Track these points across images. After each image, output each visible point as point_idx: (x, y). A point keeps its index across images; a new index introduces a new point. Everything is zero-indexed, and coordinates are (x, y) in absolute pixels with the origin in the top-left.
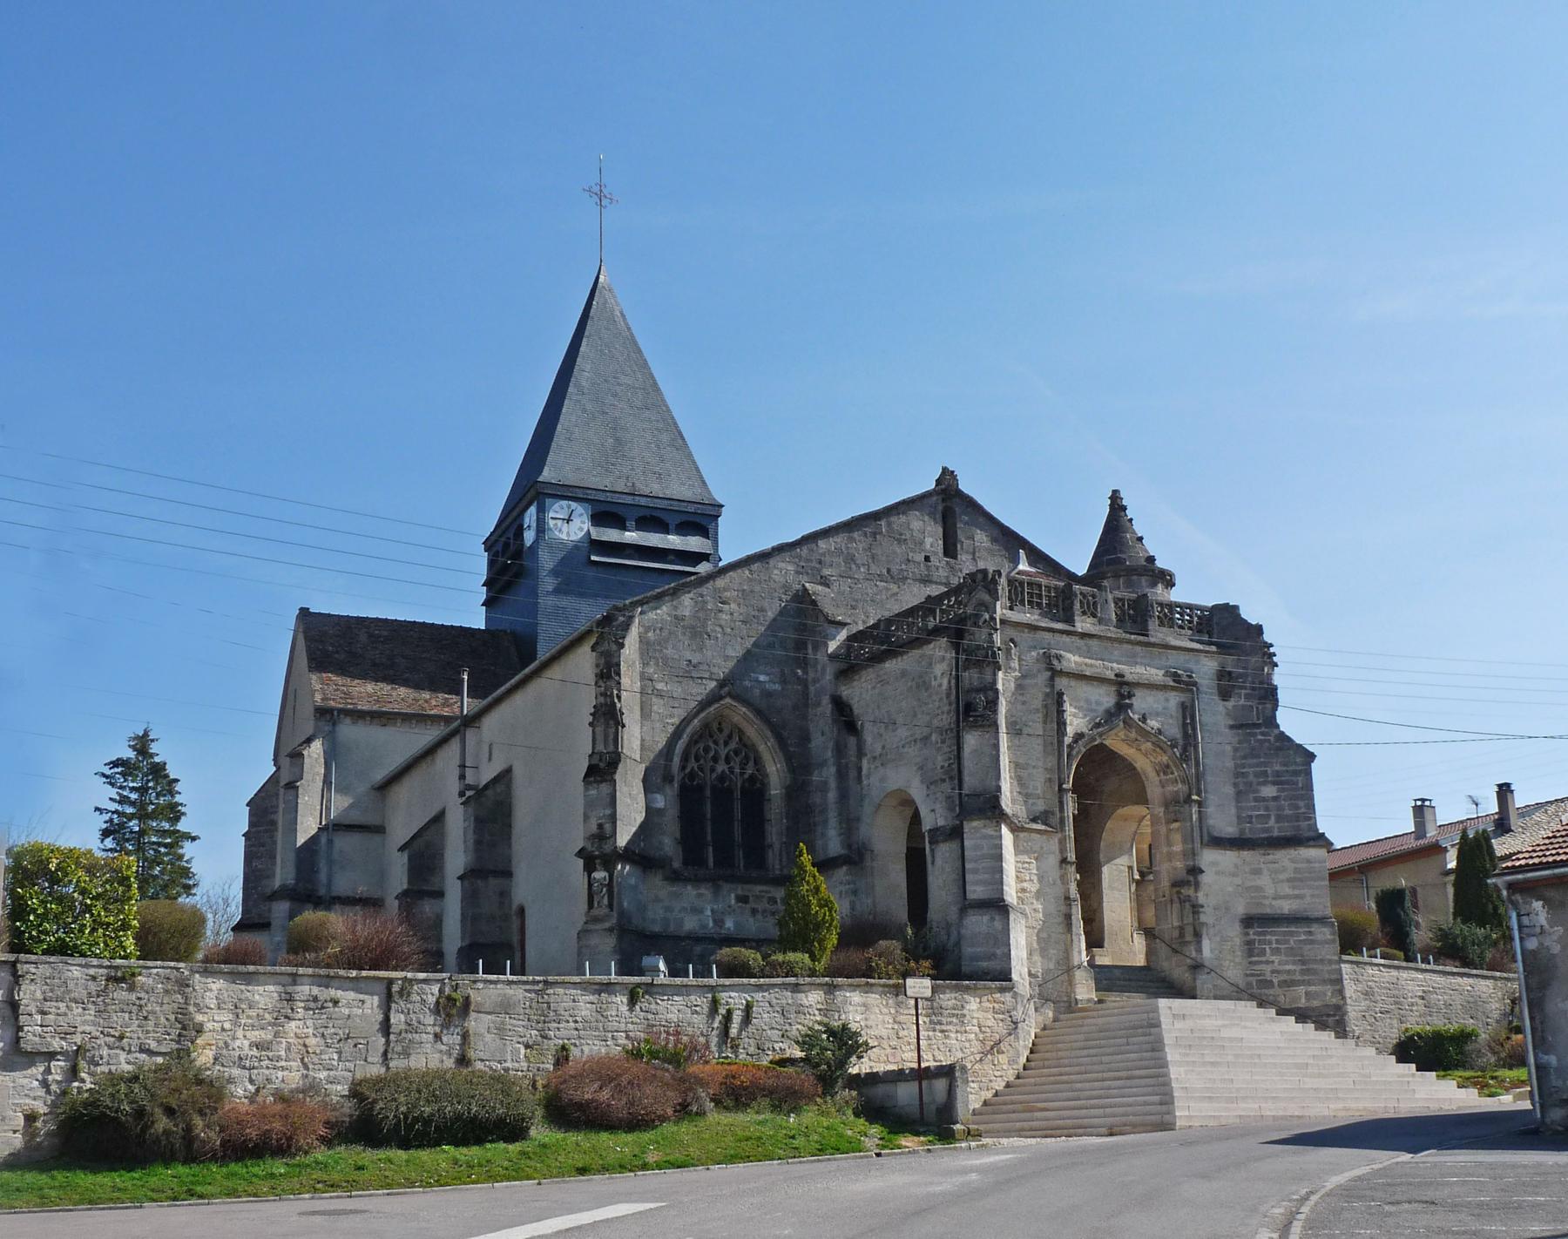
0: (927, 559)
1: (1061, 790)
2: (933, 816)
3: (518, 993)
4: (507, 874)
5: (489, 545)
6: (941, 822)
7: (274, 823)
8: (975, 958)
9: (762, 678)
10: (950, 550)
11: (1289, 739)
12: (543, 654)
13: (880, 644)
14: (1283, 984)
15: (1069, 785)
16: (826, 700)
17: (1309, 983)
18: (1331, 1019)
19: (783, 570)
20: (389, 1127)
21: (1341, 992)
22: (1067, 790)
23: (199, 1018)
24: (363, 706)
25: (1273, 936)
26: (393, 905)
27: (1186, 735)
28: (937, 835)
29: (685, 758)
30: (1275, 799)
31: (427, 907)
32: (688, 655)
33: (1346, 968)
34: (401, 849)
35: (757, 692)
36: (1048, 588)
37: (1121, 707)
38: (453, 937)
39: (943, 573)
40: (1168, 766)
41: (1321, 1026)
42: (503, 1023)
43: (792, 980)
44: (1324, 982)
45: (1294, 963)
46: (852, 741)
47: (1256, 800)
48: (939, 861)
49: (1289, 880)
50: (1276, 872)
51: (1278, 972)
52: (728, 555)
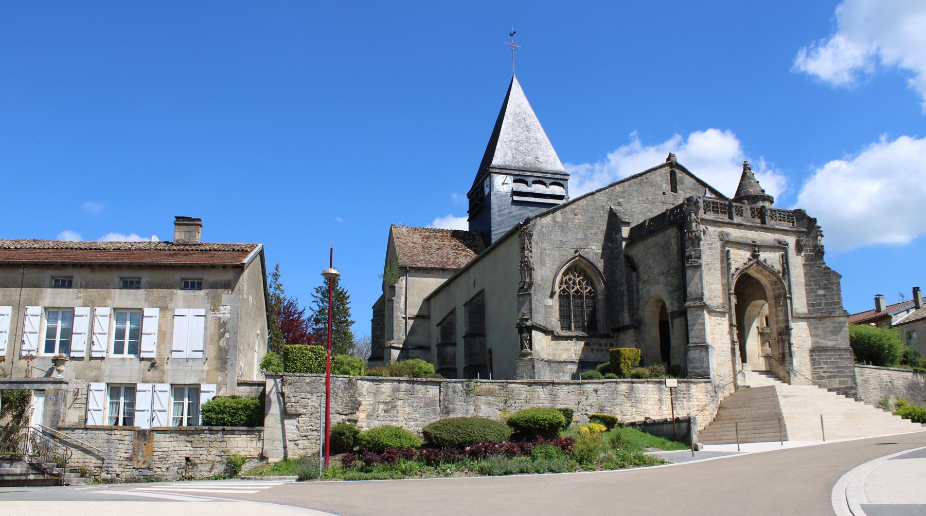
0: (664, 193)
2: (671, 307)
4: (483, 335)
5: (470, 195)
6: (676, 309)
7: (383, 315)
8: (693, 368)
10: (674, 189)
11: (829, 268)
12: (494, 239)
13: (641, 233)
15: (732, 291)
18: (849, 391)
19: (601, 198)
20: (444, 449)
21: (855, 380)
23: (360, 399)
24: (419, 265)
26: (434, 350)
27: (784, 270)
28: (674, 315)
29: (561, 283)
30: (824, 295)
31: (449, 349)
32: (561, 238)
33: (856, 369)
34: (438, 325)
35: (591, 254)
36: (721, 204)
37: (755, 256)
38: (461, 362)
39: (671, 199)
44: (847, 376)
46: (634, 275)
48: (675, 327)
49: (831, 332)
52: (572, 197)
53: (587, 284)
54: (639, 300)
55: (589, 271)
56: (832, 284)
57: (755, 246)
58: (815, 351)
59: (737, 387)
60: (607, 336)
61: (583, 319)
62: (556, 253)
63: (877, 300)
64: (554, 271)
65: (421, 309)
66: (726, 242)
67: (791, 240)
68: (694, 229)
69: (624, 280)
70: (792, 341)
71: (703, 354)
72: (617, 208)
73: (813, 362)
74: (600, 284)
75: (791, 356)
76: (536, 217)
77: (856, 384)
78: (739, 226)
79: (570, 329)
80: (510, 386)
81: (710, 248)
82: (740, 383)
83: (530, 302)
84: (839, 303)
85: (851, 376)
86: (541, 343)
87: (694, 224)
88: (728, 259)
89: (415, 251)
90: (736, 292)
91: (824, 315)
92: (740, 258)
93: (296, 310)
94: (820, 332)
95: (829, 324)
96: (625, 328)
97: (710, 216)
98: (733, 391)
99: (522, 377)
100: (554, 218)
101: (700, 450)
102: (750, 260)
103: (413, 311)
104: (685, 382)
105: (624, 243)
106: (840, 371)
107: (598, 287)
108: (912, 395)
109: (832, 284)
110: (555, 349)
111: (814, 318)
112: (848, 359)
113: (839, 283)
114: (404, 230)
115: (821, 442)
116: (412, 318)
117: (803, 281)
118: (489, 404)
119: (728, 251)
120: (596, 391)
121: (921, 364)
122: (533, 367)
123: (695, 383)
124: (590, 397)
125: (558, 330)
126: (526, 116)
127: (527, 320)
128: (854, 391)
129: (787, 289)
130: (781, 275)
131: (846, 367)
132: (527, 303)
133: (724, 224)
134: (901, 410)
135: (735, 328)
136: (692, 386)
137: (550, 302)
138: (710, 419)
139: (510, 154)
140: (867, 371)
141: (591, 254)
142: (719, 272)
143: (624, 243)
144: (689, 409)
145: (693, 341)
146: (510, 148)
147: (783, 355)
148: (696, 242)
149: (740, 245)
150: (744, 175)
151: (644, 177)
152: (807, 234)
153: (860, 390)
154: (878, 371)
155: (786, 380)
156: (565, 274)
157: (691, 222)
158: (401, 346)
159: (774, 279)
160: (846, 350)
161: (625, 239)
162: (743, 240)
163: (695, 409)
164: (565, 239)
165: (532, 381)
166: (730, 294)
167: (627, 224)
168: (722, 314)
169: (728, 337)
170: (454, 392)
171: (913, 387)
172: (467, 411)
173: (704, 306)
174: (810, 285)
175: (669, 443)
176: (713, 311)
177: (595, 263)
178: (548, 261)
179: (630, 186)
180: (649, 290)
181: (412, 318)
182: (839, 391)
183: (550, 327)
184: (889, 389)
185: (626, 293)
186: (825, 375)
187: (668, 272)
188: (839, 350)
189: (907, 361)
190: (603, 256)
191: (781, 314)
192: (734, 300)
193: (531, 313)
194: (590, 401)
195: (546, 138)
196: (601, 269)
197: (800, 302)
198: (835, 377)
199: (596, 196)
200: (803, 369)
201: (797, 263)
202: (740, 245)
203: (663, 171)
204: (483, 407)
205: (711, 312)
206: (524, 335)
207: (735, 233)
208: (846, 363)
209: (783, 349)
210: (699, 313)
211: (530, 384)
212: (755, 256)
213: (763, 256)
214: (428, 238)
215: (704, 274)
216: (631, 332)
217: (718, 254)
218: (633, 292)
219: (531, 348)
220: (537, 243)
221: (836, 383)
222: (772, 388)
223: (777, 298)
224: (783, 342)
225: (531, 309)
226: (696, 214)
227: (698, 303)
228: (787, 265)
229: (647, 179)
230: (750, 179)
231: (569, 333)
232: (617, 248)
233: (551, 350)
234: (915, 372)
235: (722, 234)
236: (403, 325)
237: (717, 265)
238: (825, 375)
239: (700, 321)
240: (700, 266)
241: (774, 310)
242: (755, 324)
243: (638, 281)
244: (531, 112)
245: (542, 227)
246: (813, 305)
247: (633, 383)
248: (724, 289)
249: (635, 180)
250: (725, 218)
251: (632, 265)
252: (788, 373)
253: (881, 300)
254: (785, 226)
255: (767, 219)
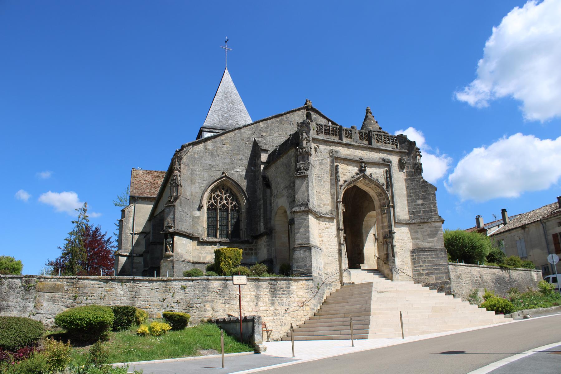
1: (338, 202)
3: (64, 283)
8: (298, 267)
9: (238, 170)
11: (426, 182)
14: (427, 274)
15: (341, 199)
16: (260, 177)
17: (437, 274)
18: (444, 287)
22: (339, 202)
24: (145, 195)
25: (422, 256)
27: (387, 183)
30: (422, 204)
33: (450, 267)
35: (236, 175)
37: (362, 170)
40: (381, 193)
41: (440, 290)
42: (55, 297)
43: (223, 277)
44: (442, 273)
45: (431, 266)
46: (268, 191)
47: (415, 205)
49: (428, 235)
50: (424, 232)
51: (425, 270)
53: (233, 200)
54: (271, 212)
55: (234, 189)
56: (429, 195)
57: (362, 162)
58: (416, 252)
59: (342, 284)
60: (247, 242)
61: (228, 228)
62: (205, 174)
63: (478, 220)
64: (203, 189)
65: (145, 227)
66: (335, 158)
67: (395, 160)
68: (305, 145)
69: (261, 196)
70: (394, 243)
71: (307, 253)
72: (260, 139)
73: (414, 261)
74: (243, 199)
75: (393, 256)
76: (189, 145)
77: (450, 279)
78: (348, 145)
79: (216, 236)
80: (81, 282)
81: (320, 163)
82: (345, 280)
83: (174, 212)
84: (435, 211)
85: (446, 273)
86: (183, 248)
87: (305, 142)
88: (337, 173)
89: (145, 186)
90: (344, 201)
91: (422, 221)
92: (348, 172)
93: (100, 233)
94: (419, 235)
95: (426, 228)
96: (261, 235)
97: (322, 137)
98: (339, 288)
99: (165, 276)
100: (205, 146)
101: (263, 353)
102: (357, 174)
103: (139, 228)
104: (285, 280)
105: (262, 167)
106: (436, 268)
107: (241, 202)
108: (498, 288)
109: (429, 195)
110: (200, 253)
111: (413, 224)
112: (443, 258)
113: (434, 194)
114: (141, 172)
115: (399, 341)
116: (138, 234)
117: (405, 193)
118: (54, 301)
119: (337, 166)
120: (184, 288)
121: (505, 262)
122: (173, 267)
123: (295, 281)
124: (176, 294)
125: (205, 237)
126: (232, 95)
127: (170, 227)
128: (448, 286)
129: (390, 198)
130: (385, 187)
131: (442, 265)
132: (172, 213)
133: (334, 143)
134: (488, 303)
135: (342, 232)
136: (293, 283)
137: (197, 213)
138: (311, 314)
139: (217, 119)
140: (460, 268)
141: (236, 175)
142: (329, 183)
143: (262, 167)
144: (289, 304)
145: (298, 242)
146: (218, 115)
147: (387, 255)
148: (306, 156)
149: (348, 161)
150: (366, 117)
151: (284, 117)
152: (408, 154)
153: (454, 286)
154: (469, 268)
155: (389, 277)
156: (213, 191)
157: (302, 140)
158: (128, 254)
159: (380, 190)
160: (441, 250)
161: (263, 163)
162: (352, 158)
163: (296, 304)
164: (214, 163)
165: (109, 277)
166: (338, 202)
167: (266, 151)
168: (331, 219)
169: (336, 239)
170: (10, 288)
171: (499, 281)
172: (25, 309)
173: (309, 212)
174: (411, 196)
175: (236, 344)
176: (322, 217)
177: (240, 183)
178: (198, 181)
179: (272, 123)
180: (277, 203)
181: (138, 234)
182: (432, 286)
183: (196, 235)
184: (479, 283)
185: (262, 206)
186: (424, 272)
187: (289, 186)
188: (436, 250)
189: (492, 259)
190: (246, 177)
191: (386, 220)
192: (342, 208)
193: (174, 221)
194: (176, 298)
195: (245, 109)
196: (245, 188)
197: (402, 210)
198: (432, 274)
199: (243, 130)
200: (405, 267)
201: (400, 179)
202: (348, 161)
203: (300, 112)
204: (45, 304)
205: (318, 217)
206: (168, 240)
207: (343, 152)
208: (442, 262)
209: (387, 250)
210: (304, 217)
211: (106, 281)
212: (362, 170)
213: (369, 171)
214: (157, 177)
215: (310, 184)
216: (264, 238)
217: (328, 169)
218: (268, 205)
219: (173, 251)
220: (188, 165)
221: (433, 279)
222: (370, 284)
223: (382, 207)
224: (387, 244)
225: (174, 218)
226: (307, 133)
227: (303, 209)
228: (391, 179)
229: (287, 118)
230: (370, 119)
231: (215, 240)
232: (258, 171)
233: (196, 253)
234: (501, 268)
235: (332, 151)
236: (130, 239)
237: (327, 177)
238: (424, 272)
239: (305, 224)
240: (307, 176)
241: (380, 217)
242: (372, 231)
243: (271, 196)
244: (236, 92)
245: (195, 153)
246: (413, 213)
247: (227, 280)
248: (332, 198)
249: (277, 119)
250: (336, 139)
251: (267, 184)
252: (391, 271)
253: (480, 220)
254: (390, 147)
255: (374, 141)
